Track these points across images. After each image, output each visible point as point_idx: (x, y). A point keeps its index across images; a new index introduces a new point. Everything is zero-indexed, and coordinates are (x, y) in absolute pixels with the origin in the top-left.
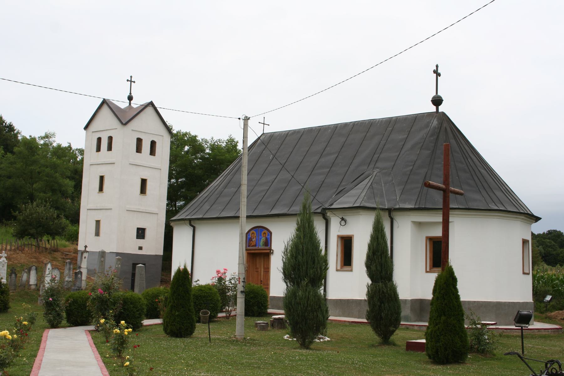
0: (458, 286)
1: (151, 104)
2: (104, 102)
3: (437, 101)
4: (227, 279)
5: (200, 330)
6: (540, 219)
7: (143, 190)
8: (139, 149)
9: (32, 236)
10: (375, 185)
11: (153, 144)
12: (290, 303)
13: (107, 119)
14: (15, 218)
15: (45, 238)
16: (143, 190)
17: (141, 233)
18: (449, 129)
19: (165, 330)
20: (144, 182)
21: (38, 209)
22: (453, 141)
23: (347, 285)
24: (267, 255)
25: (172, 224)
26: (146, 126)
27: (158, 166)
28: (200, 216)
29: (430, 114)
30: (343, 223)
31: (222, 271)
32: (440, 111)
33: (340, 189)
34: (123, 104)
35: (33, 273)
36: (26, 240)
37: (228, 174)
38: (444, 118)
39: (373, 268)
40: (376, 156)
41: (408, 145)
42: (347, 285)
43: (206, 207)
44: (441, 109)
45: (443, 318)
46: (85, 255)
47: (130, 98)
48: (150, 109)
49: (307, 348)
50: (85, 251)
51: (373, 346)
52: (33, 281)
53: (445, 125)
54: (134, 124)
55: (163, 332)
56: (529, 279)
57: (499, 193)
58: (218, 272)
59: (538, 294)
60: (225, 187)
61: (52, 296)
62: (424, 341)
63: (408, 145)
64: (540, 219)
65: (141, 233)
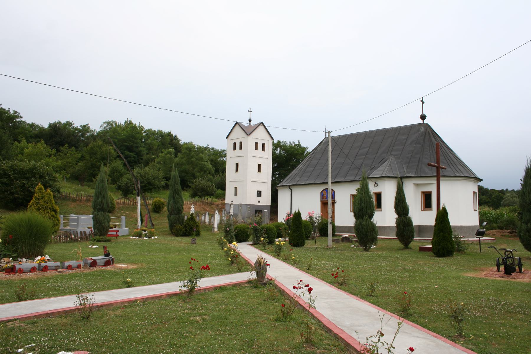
0: (449, 217)
1: (262, 123)
2: (237, 123)
3: (423, 117)
4: (315, 217)
5: (309, 244)
6: (482, 180)
7: (259, 170)
8: (256, 148)
9: (200, 197)
10: (392, 165)
11: (264, 145)
12: (359, 228)
13: (238, 133)
14: (190, 187)
15: (206, 198)
16: (259, 170)
17: (259, 193)
18: (430, 133)
19: (290, 243)
20: (259, 166)
21: (201, 182)
22: (433, 139)
23: (385, 218)
24: (327, 203)
25: (278, 188)
26: (260, 135)
27: (267, 157)
28: (295, 184)
29: (419, 125)
30: (376, 185)
31: (312, 213)
32: (425, 122)
33: (372, 167)
34: (246, 123)
35: (207, 216)
36: (197, 198)
37: (308, 160)
38: (427, 126)
39: (399, 209)
40: (391, 148)
41: (409, 142)
42: (385, 218)
43: (297, 178)
44: (425, 121)
45: (442, 234)
46: (232, 206)
47: (250, 121)
48: (261, 127)
49: (368, 251)
50: (232, 204)
51: (399, 250)
52: (207, 220)
53: (429, 130)
54: (254, 135)
55: (289, 245)
56: (477, 214)
57: (460, 167)
58: (310, 213)
59: (481, 222)
60: (307, 167)
61: (228, 227)
62: (431, 246)
63: (409, 142)
64: (482, 180)
65: (259, 193)
